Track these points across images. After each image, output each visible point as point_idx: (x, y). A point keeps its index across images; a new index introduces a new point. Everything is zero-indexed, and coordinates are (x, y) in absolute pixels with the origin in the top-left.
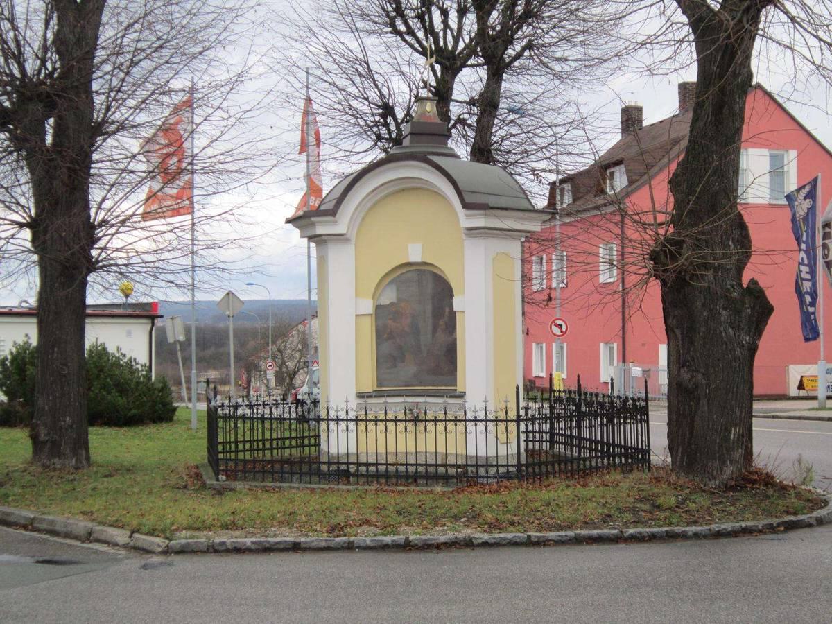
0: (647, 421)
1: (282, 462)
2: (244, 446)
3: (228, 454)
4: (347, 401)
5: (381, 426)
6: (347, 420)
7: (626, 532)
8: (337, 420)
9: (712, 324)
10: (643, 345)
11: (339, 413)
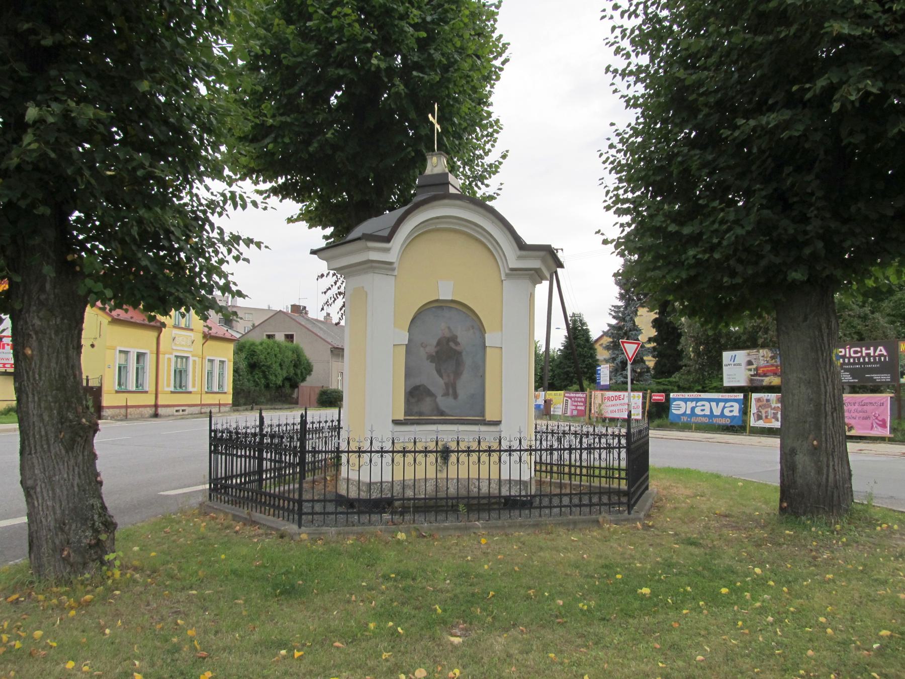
0: (211, 431)
1: (591, 492)
2: (600, 473)
3: (597, 480)
4: (520, 432)
5: (474, 457)
6: (520, 450)
7: (197, 83)
8: (360, 452)
9: (824, 671)
10: (112, 643)
11: (384, 445)
